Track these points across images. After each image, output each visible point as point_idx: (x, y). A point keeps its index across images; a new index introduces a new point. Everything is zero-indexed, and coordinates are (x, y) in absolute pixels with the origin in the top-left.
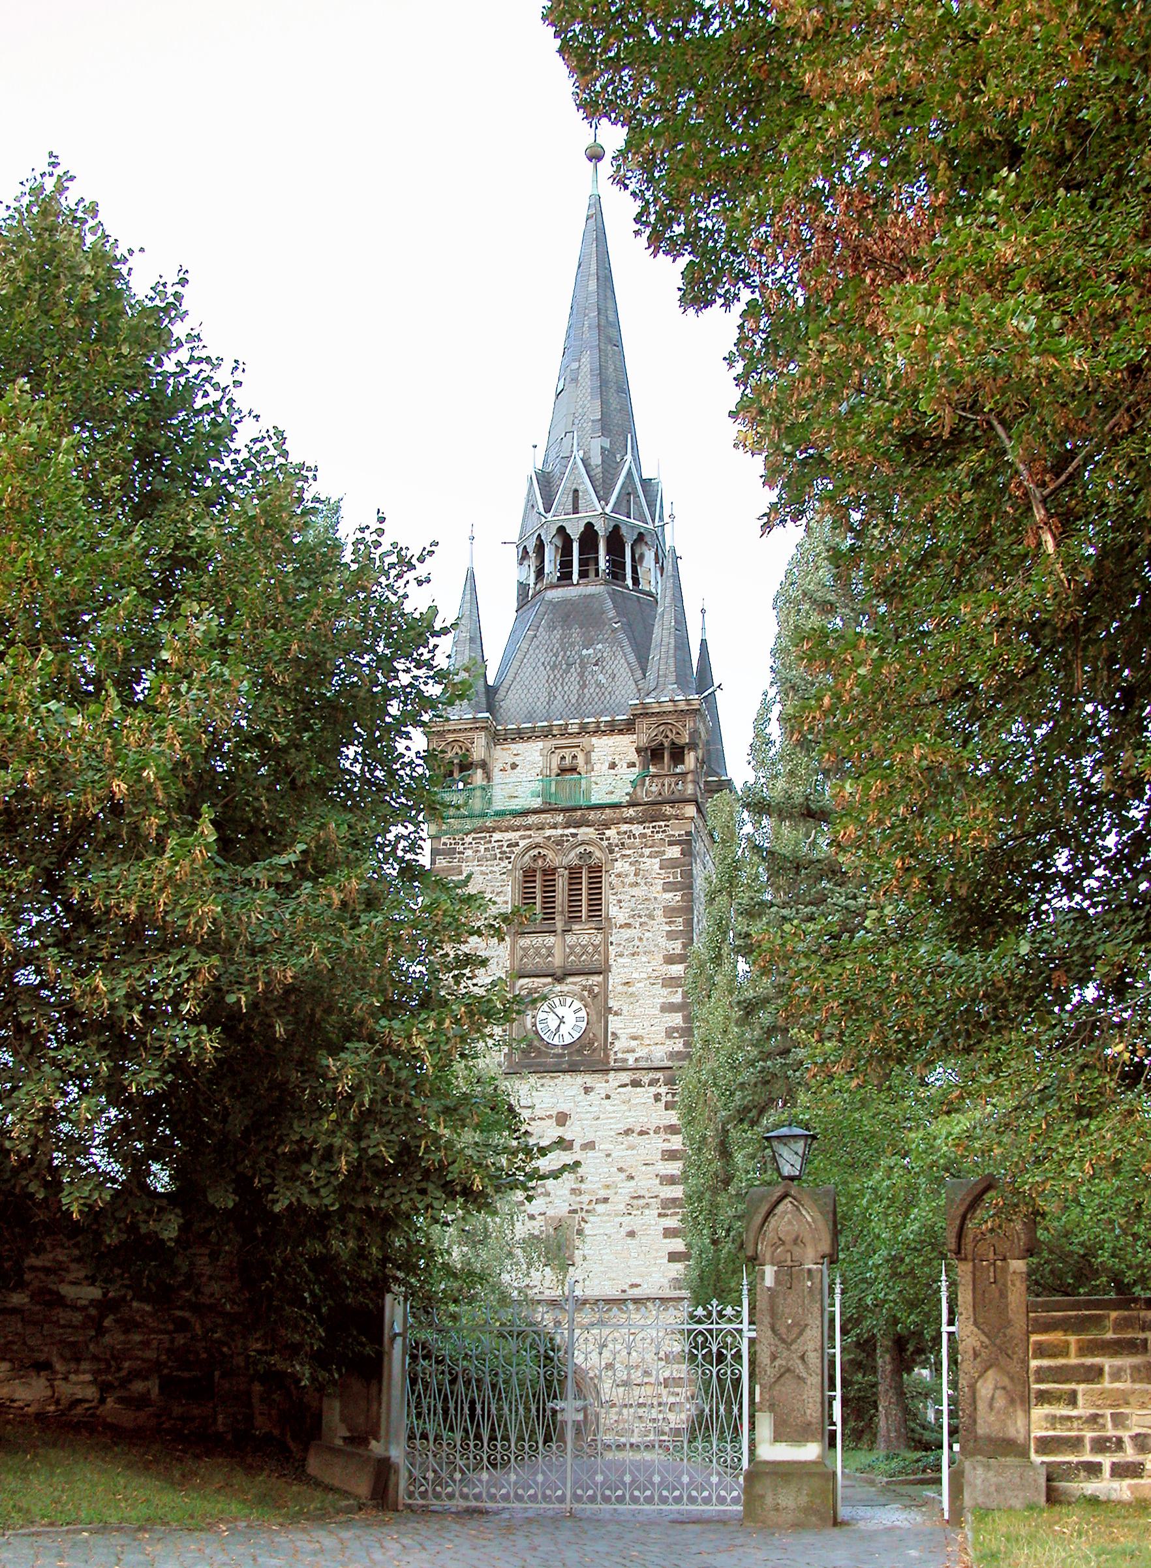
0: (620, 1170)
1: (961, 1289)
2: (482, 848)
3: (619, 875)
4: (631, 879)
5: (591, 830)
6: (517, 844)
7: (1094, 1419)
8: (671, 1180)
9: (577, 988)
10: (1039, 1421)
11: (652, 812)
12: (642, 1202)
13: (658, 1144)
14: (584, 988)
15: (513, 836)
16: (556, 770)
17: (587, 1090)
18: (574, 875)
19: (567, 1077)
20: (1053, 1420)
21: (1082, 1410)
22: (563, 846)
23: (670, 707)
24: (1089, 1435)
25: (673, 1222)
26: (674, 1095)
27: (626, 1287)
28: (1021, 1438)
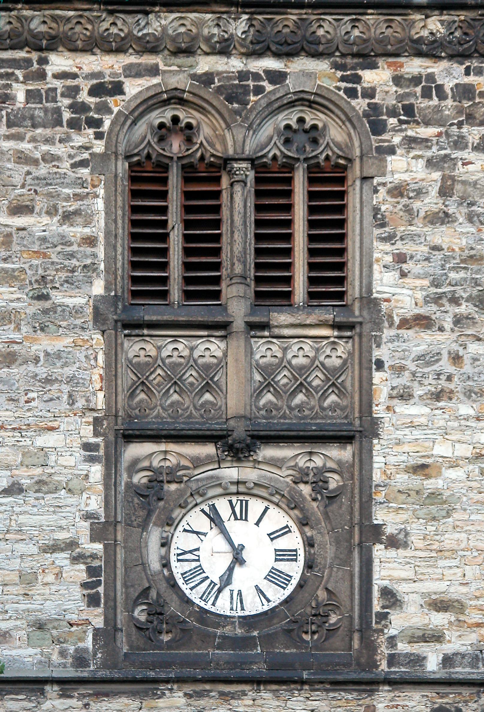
3: (398, 191)
4: (431, 202)
5: (321, 66)
6: (117, 89)
9: (283, 476)
14: (302, 476)
15: (108, 64)
18: (271, 183)
19: (266, 695)
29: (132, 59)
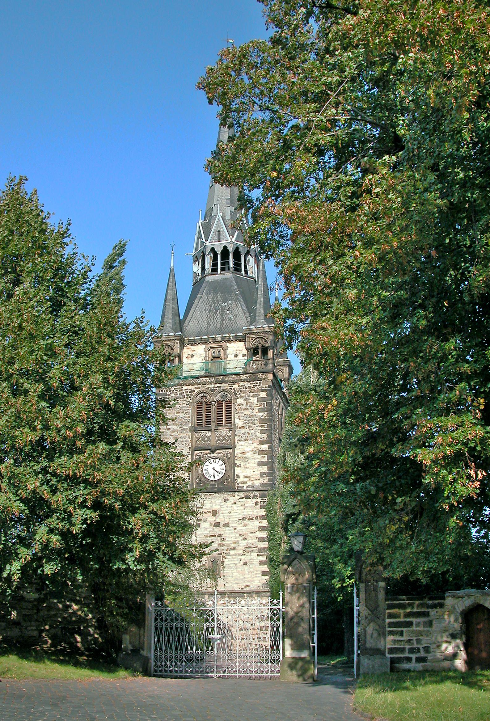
0: (240, 535)
1: (361, 593)
2: (178, 393)
3: (239, 405)
4: (245, 406)
7: (409, 641)
8: (261, 540)
9: (221, 455)
10: (389, 641)
11: (253, 377)
12: (250, 549)
13: (257, 524)
16: (211, 358)
17: (226, 500)
18: (219, 404)
19: (217, 494)
20: (394, 641)
21: (405, 638)
22: (216, 391)
23: (261, 330)
24: (407, 647)
25: (264, 558)
26: (264, 502)
27: (243, 587)
28: (383, 648)
29: (196, 386)
